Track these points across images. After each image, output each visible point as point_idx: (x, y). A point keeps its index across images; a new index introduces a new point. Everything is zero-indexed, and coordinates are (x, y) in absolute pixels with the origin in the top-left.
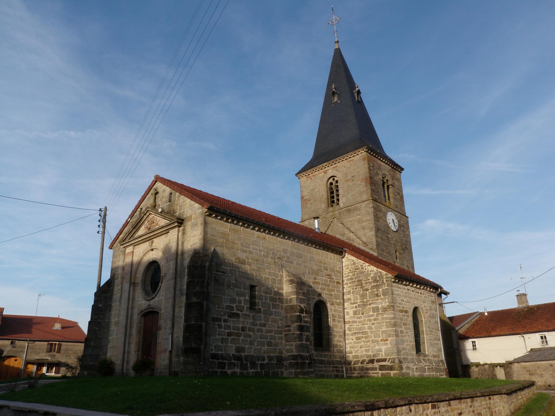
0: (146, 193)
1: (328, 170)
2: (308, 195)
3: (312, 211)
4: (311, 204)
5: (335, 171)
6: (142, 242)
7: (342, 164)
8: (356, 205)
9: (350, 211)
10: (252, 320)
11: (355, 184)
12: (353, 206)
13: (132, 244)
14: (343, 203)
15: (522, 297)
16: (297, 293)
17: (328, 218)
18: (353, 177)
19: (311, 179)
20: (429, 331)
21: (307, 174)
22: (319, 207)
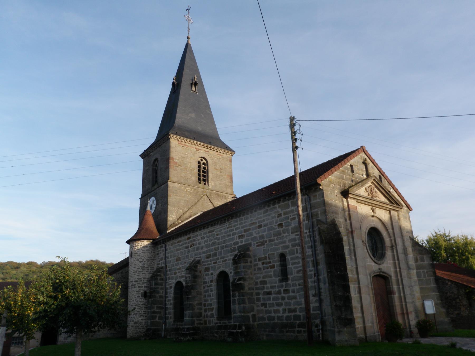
0: (375, 164)
1: (200, 150)
2: (178, 160)
3: (182, 177)
4: (181, 169)
5: (207, 155)
6: (367, 203)
7: (214, 153)
8: (224, 194)
9: (219, 196)
10: (167, 321)
11: (222, 176)
12: (221, 193)
13: (358, 199)
14: (212, 186)
15: (418, 333)
16: (448, 314)
17: (199, 192)
18: (221, 169)
19: (183, 146)
20: (19, 345)
21: (180, 140)
22: (189, 177)
